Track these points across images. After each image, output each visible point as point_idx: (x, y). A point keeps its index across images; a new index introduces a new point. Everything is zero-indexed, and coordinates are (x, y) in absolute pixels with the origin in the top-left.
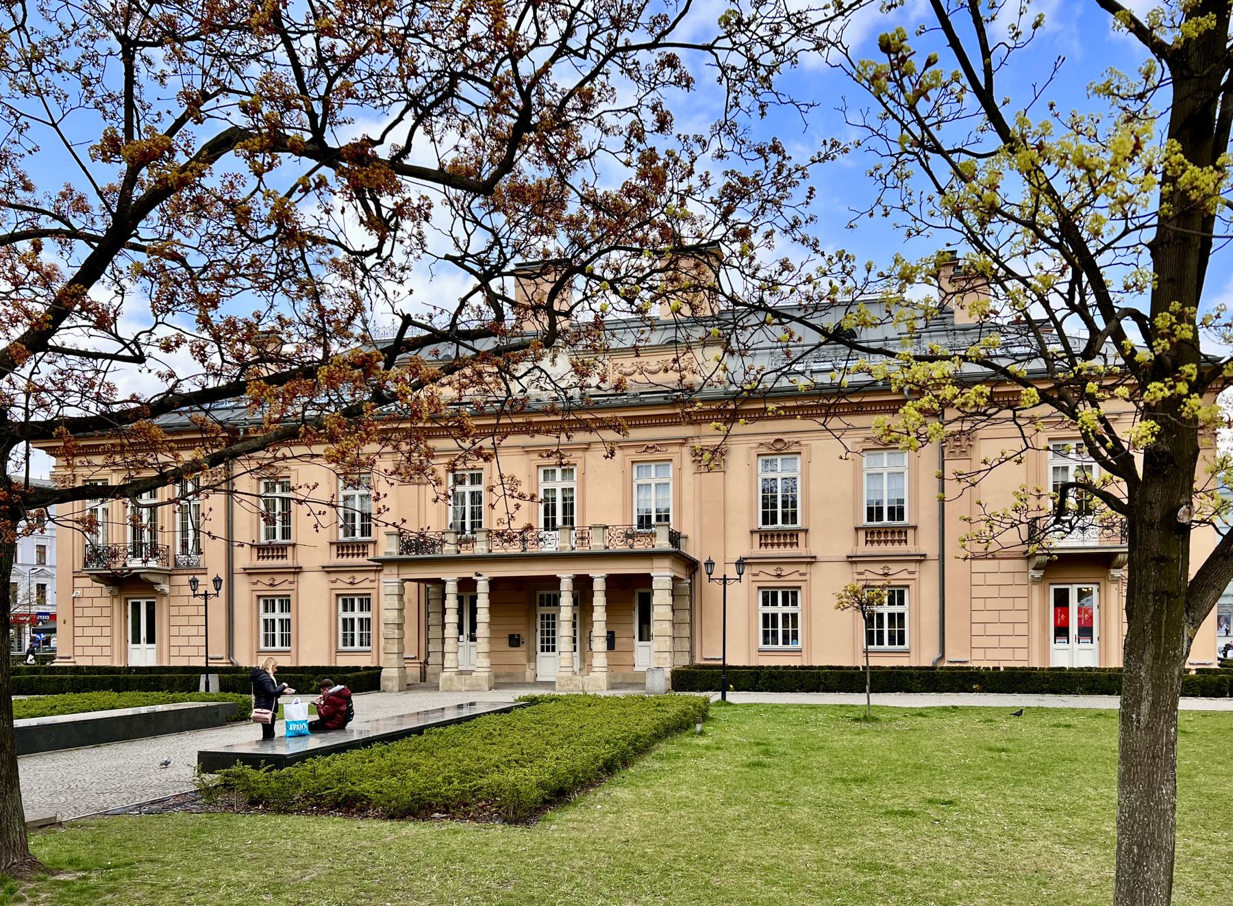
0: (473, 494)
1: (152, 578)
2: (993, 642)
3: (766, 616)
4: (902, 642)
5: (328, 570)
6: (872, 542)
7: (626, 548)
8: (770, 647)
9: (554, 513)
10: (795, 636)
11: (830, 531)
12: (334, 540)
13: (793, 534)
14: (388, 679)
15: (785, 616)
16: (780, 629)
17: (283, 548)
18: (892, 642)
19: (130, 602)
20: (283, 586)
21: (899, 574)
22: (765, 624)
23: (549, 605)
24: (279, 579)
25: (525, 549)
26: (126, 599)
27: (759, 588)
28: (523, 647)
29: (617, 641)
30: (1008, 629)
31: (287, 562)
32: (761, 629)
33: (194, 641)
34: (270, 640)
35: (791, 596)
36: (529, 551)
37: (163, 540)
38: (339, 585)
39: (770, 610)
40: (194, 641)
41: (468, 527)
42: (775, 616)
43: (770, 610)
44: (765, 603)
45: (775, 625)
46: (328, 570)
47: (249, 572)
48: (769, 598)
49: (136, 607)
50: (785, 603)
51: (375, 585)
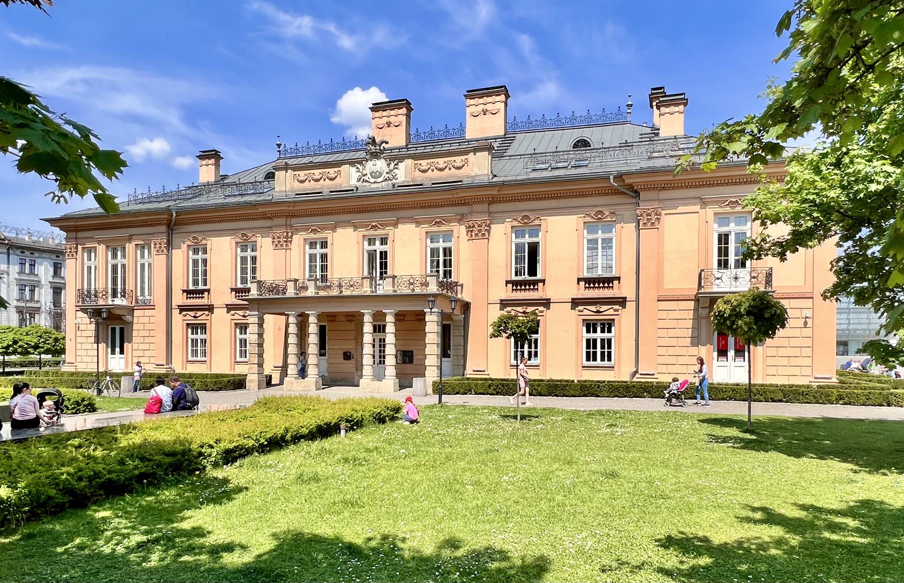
0: (445, 249)
1: (119, 312)
2: (784, 361)
3: (588, 341)
4: (609, 359)
5: (230, 308)
6: (589, 288)
7: (409, 292)
8: (591, 363)
9: (381, 263)
10: (536, 355)
11: (560, 277)
12: (509, 279)
13: (535, 283)
14: (251, 381)
15: (603, 340)
16: (599, 350)
17: (202, 292)
18: (603, 359)
19: (110, 327)
20: (203, 317)
21: (608, 311)
22: (588, 347)
23: (379, 332)
24: (199, 313)
25: (341, 292)
26: (108, 326)
27: (584, 320)
28: (353, 361)
29: (415, 357)
30: (796, 352)
31: (204, 301)
32: (585, 350)
33: (90, 353)
34: (194, 353)
35: (608, 326)
36: (344, 293)
37: (130, 286)
38: (188, 317)
39: (592, 335)
40: (90, 353)
41: (441, 273)
42: (595, 341)
43: (592, 335)
44: (588, 331)
45: (595, 347)
46: (575, 303)
47: (182, 309)
48: (590, 326)
49: (113, 330)
50: (603, 331)
51: (209, 318)
